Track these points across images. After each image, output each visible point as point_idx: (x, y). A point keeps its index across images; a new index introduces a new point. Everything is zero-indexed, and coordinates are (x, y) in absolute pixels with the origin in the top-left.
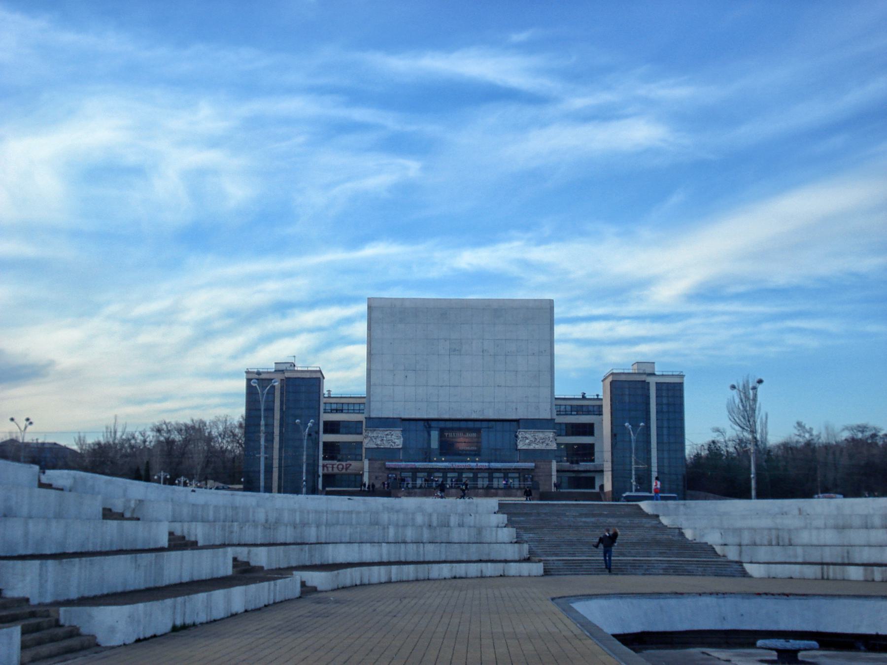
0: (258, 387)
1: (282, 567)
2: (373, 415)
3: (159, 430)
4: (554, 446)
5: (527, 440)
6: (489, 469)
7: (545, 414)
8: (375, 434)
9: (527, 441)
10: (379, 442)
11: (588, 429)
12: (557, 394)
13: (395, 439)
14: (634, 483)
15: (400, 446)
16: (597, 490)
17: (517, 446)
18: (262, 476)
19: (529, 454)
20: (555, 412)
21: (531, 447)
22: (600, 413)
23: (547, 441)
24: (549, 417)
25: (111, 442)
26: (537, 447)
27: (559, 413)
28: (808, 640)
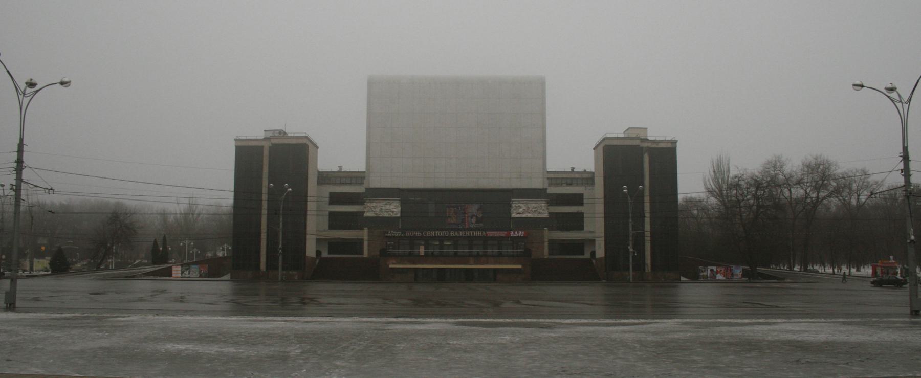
0: (247, 158)
1: (24, 154)
2: (372, 186)
3: (280, 133)
4: (546, 215)
5: (521, 209)
6: (469, 237)
8: (374, 204)
9: (521, 210)
11: (577, 199)
12: (551, 167)
13: (393, 209)
14: (631, 250)
15: (399, 215)
16: (587, 255)
17: (510, 213)
18: (501, 320)
19: (523, 223)
20: (547, 182)
21: (524, 216)
22: (593, 183)
23: (538, 210)
24: (541, 187)
25: (840, 204)
26: (530, 215)
27: (550, 185)
28: (436, 317)
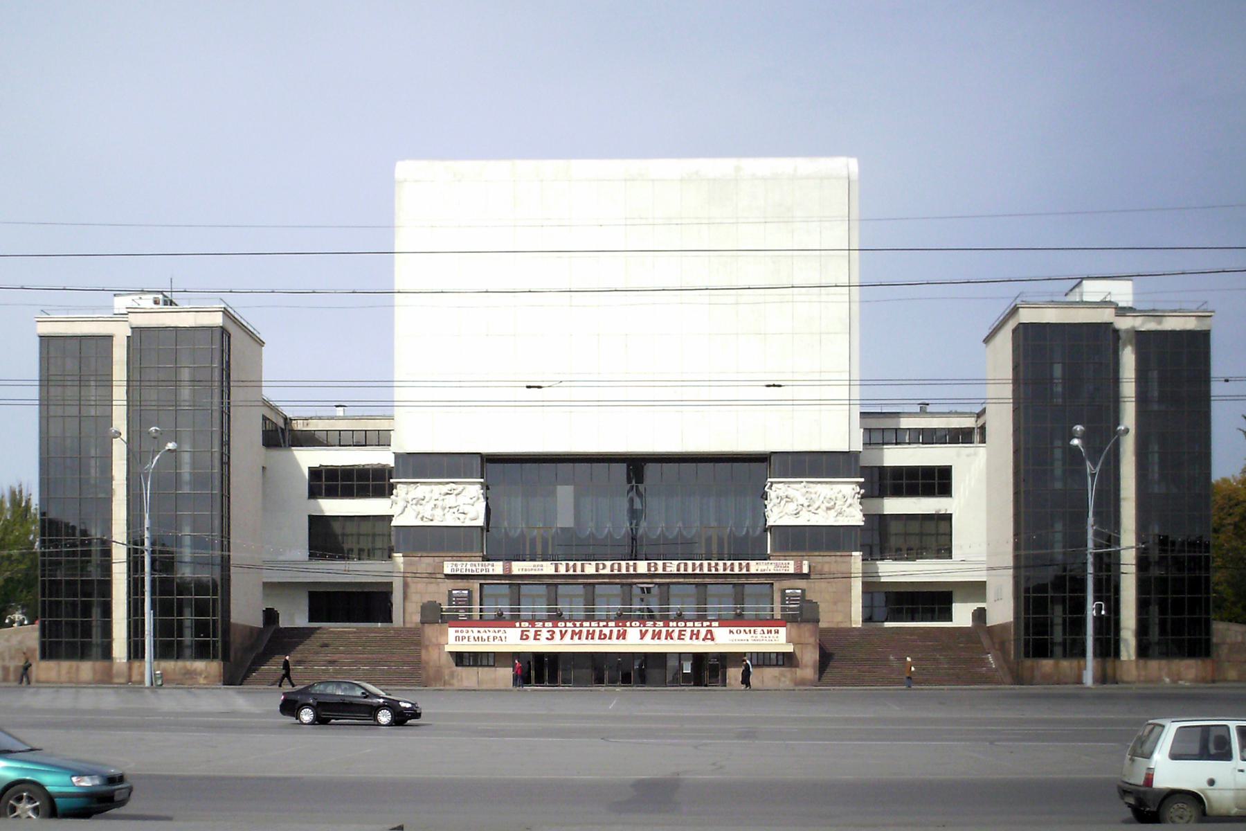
4: (855, 517)
5: (792, 504)
7: (837, 432)
10: (428, 514)
19: (799, 539)
23: (837, 504)
